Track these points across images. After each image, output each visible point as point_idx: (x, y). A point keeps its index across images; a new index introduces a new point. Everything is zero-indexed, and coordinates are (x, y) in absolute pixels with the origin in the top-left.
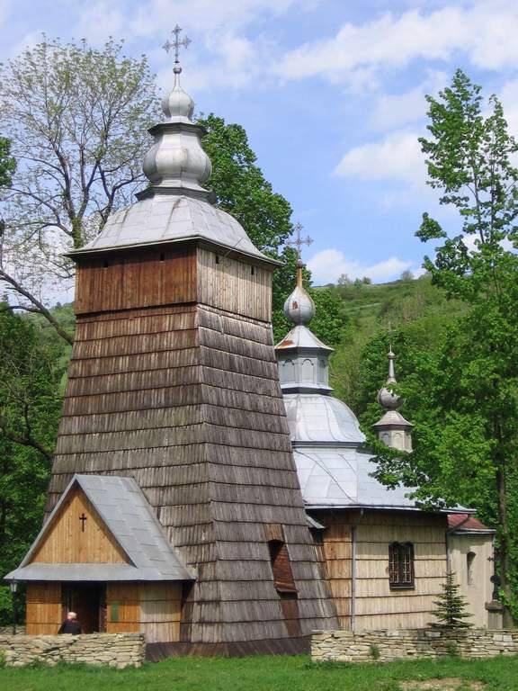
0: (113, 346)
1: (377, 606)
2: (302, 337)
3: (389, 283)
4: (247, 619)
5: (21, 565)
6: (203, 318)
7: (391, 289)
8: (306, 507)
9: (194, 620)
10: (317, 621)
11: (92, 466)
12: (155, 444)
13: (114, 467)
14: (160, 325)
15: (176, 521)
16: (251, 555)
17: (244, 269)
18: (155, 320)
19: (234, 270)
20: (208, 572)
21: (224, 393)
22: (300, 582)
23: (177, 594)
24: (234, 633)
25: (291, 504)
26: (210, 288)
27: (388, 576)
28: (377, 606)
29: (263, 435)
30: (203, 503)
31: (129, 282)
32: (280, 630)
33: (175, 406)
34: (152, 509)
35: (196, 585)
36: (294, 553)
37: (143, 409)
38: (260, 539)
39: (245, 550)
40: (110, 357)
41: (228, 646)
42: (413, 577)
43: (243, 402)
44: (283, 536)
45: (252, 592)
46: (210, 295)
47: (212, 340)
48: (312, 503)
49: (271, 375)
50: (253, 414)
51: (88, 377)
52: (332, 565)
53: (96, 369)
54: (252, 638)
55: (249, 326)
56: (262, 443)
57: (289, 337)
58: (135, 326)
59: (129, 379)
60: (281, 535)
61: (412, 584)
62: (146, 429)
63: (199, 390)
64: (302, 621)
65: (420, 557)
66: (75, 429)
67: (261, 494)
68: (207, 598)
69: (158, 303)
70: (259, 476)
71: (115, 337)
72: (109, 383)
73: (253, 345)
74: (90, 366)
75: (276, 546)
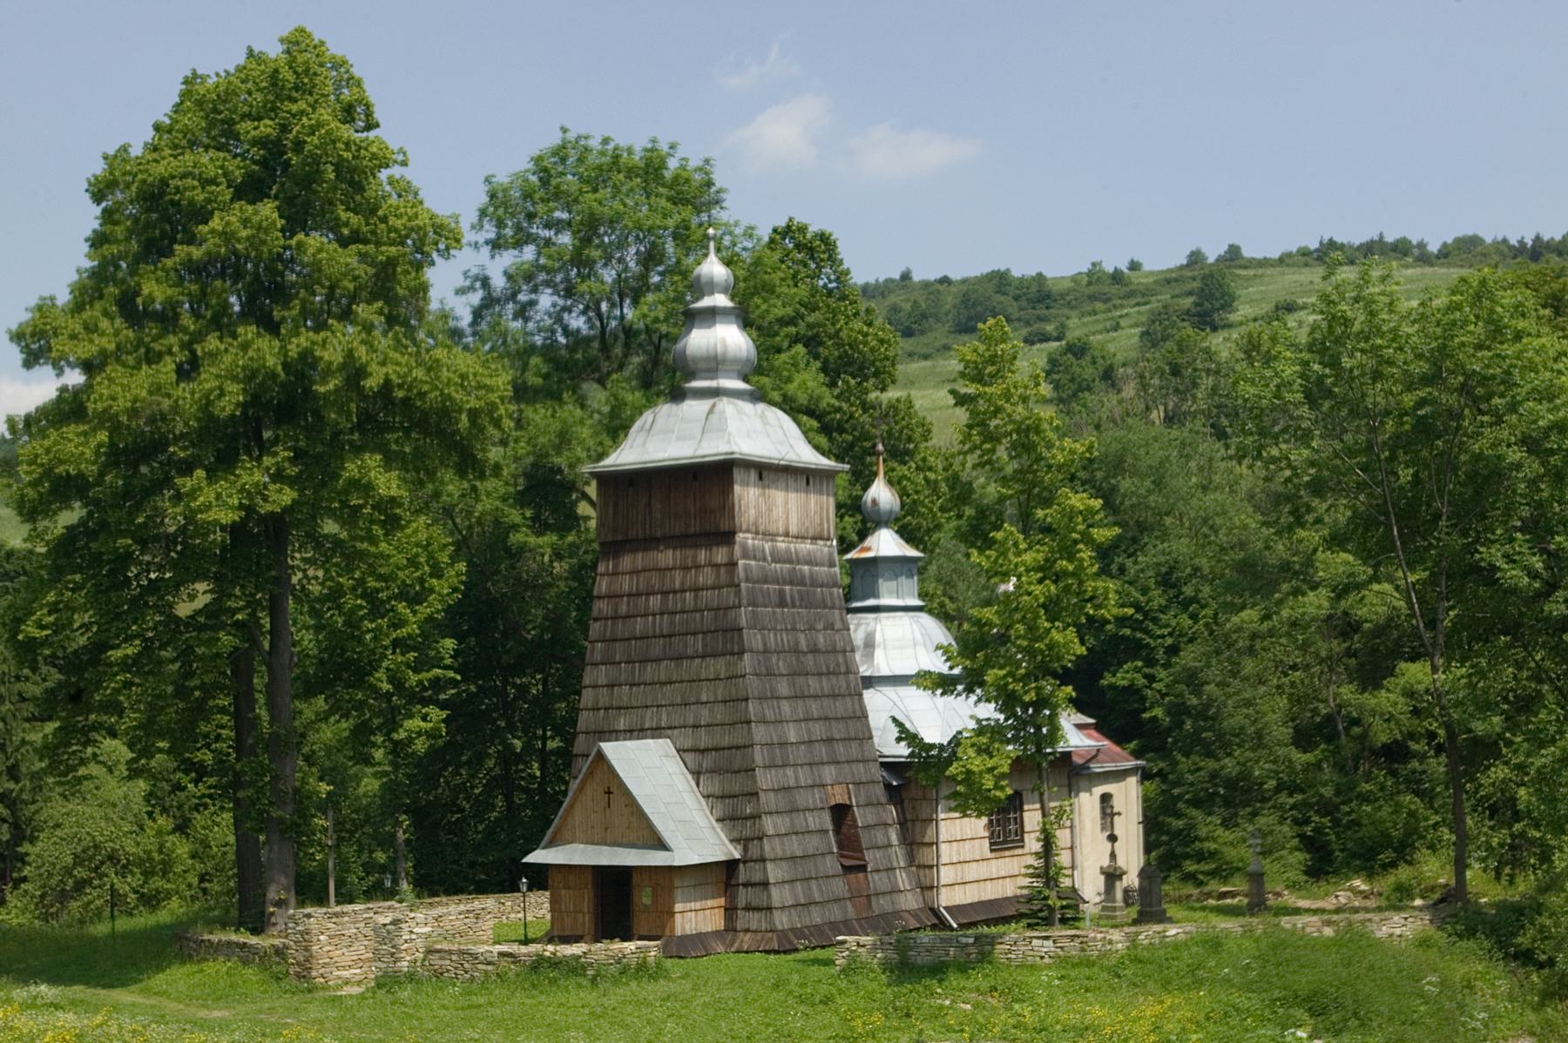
0: (642, 582)
1: (973, 872)
2: (886, 543)
3: (1162, 272)
4: (802, 901)
5: (542, 844)
6: (744, 548)
7: (1168, 282)
8: (881, 760)
9: (739, 906)
10: (894, 895)
11: (622, 723)
12: (693, 700)
13: (647, 726)
14: (695, 557)
15: (717, 791)
16: (807, 826)
17: (796, 480)
18: (690, 552)
19: (784, 485)
20: (754, 851)
21: (772, 635)
22: (871, 851)
23: (722, 876)
24: (785, 919)
25: (860, 758)
26: (752, 512)
27: (987, 834)
28: (973, 872)
29: (824, 679)
30: (746, 771)
31: (658, 506)
32: (845, 911)
33: (715, 656)
34: (689, 777)
35: (741, 865)
36: (861, 817)
37: (678, 658)
38: (819, 805)
39: (800, 821)
40: (639, 595)
41: (778, 937)
42: (1023, 832)
43: (797, 644)
44: (850, 799)
45: (810, 868)
46: (752, 520)
47: (755, 573)
48: (887, 753)
49: (833, 604)
50: (810, 656)
51: (615, 618)
52: (913, 826)
53: (623, 609)
54: (808, 924)
55: (806, 547)
56: (822, 688)
57: (869, 542)
58: (667, 557)
59: (662, 620)
60: (846, 797)
61: (1022, 840)
62: (682, 682)
63: (741, 636)
64: (874, 899)
65: (1031, 807)
66: (602, 680)
67: (822, 751)
68: (753, 881)
69: (692, 530)
70: (818, 730)
71: (644, 570)
72: (639, 625)
73: (810, 571)
74: (616, 605)
75: (841, 813)
